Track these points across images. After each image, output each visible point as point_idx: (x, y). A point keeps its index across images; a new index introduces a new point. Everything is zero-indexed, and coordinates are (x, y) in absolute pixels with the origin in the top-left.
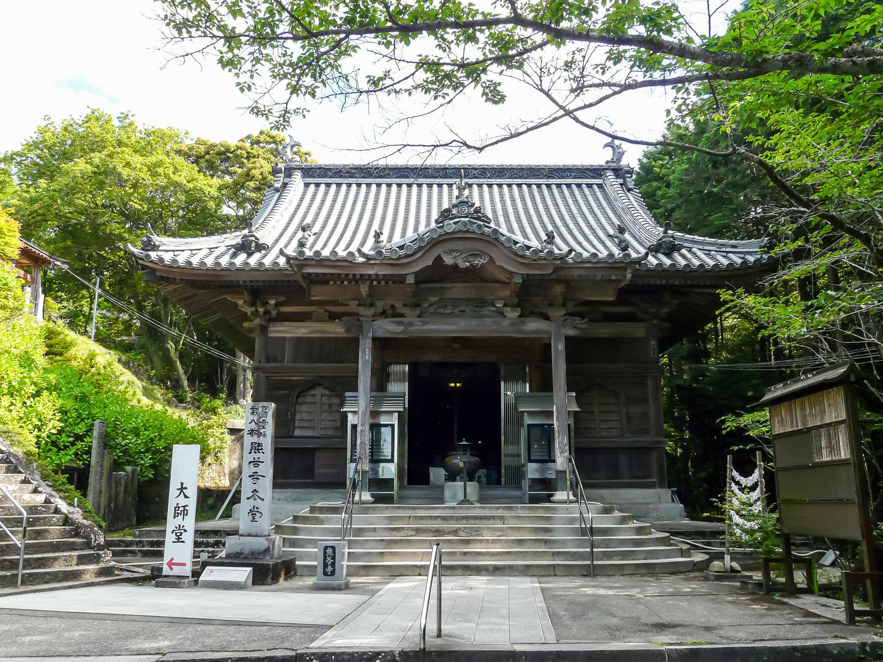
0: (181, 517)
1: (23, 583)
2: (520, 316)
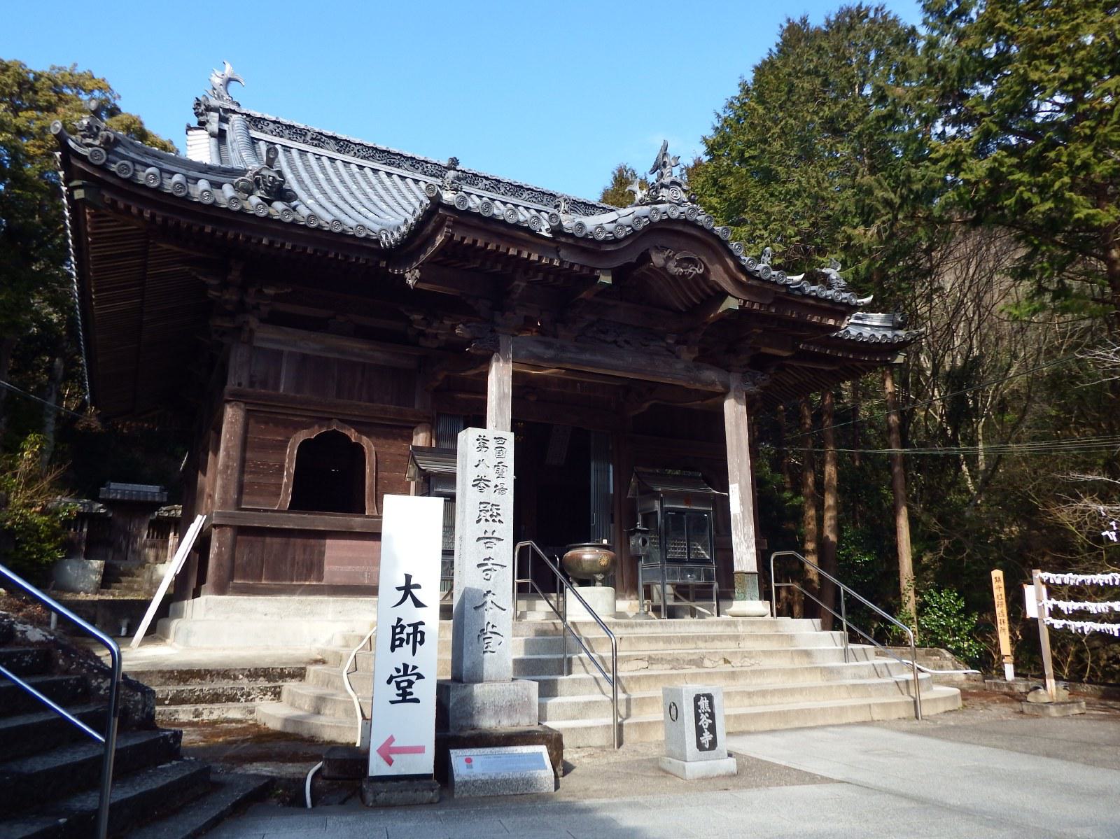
0: (407, 648)
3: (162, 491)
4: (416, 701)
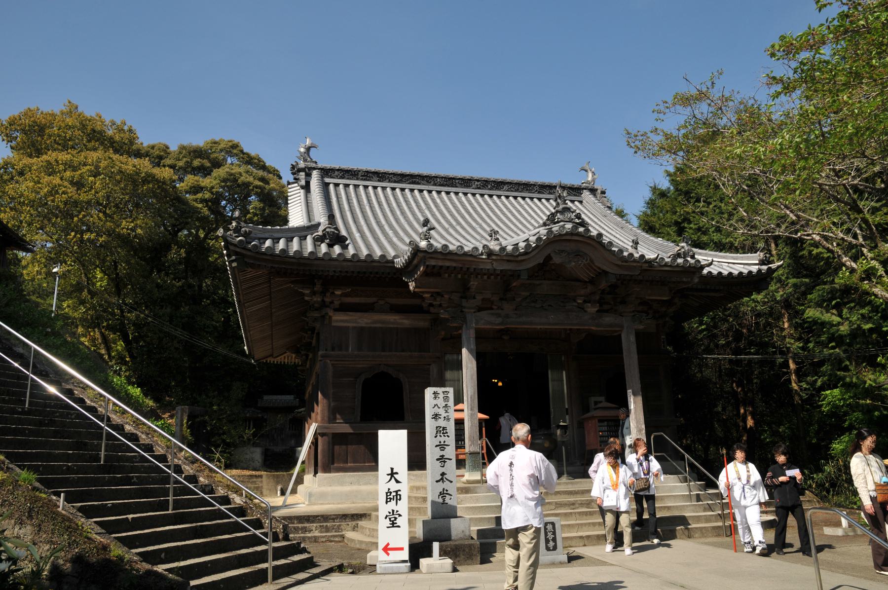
1: (275, 578)
2: (598, 311)
3: (295, 398)
4: (399, 527)
